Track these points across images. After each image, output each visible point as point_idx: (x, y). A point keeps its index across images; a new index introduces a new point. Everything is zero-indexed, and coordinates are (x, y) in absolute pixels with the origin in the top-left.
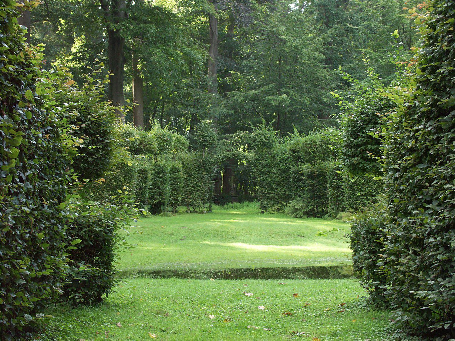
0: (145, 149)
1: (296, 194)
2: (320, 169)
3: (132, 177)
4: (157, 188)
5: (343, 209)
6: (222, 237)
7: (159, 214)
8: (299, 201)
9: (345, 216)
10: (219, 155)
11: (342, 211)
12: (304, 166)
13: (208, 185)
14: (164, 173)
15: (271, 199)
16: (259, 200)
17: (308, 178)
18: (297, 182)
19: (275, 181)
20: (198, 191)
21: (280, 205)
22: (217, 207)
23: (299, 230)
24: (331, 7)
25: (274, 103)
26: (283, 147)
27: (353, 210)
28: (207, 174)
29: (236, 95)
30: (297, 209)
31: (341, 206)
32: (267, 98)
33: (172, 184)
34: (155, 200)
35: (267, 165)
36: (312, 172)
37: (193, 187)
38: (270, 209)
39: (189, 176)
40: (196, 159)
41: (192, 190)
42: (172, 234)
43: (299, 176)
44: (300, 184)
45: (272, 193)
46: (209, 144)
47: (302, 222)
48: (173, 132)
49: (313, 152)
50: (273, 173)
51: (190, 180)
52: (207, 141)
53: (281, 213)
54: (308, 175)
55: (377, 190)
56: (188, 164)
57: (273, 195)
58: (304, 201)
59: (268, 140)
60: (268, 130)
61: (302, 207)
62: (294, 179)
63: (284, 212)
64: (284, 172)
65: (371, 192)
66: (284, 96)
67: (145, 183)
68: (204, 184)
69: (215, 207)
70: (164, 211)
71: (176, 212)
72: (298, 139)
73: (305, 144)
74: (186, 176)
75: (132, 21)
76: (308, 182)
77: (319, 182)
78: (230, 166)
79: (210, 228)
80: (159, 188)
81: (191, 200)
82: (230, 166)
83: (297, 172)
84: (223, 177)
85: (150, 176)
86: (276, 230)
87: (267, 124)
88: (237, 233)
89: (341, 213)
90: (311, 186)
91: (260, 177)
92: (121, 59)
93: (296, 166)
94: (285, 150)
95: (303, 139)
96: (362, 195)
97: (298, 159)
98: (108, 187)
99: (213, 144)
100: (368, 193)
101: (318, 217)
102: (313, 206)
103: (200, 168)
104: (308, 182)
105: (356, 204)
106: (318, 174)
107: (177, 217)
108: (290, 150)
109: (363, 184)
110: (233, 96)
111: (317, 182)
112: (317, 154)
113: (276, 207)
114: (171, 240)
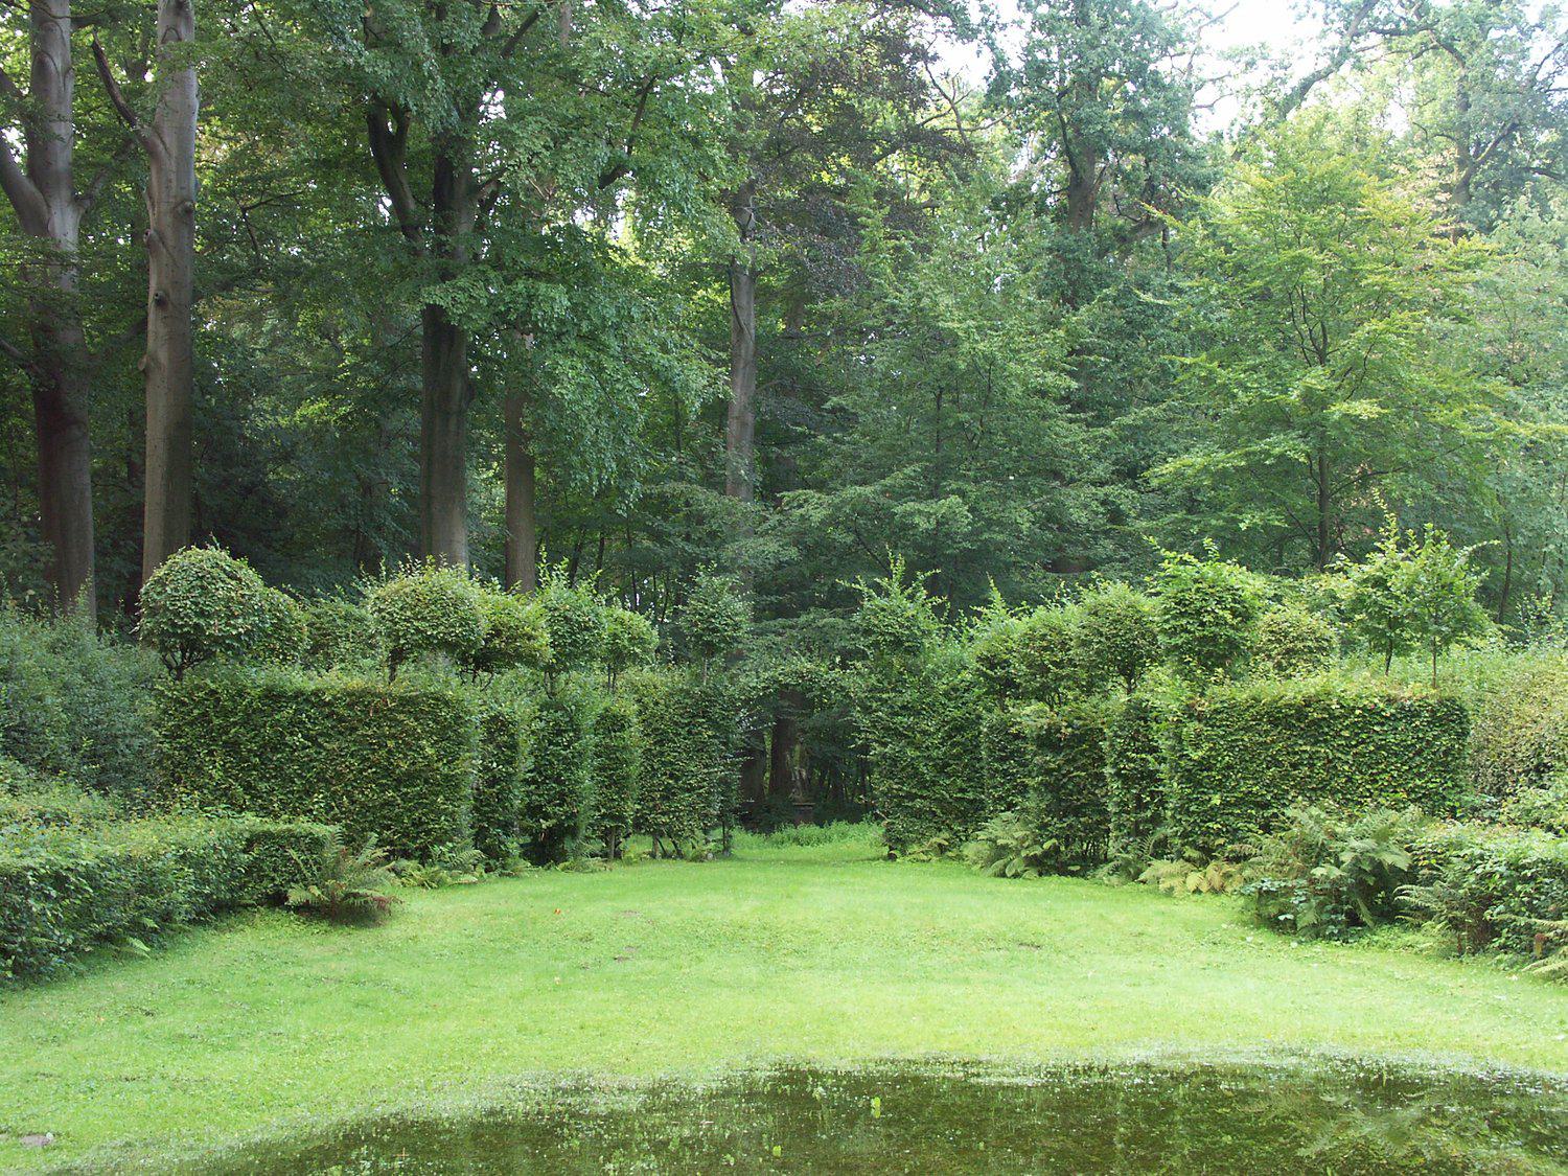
0: (511, 652)
1: (1001, 798)
2: (1079, 718)
3: (461, 743)
4: (550, 775)
5: (1161, 850)
6: (759, 949)
7: (557, 863)
8: (1008, 822)
9: (1172, 875)
10: (752, 678)
11: (1158, 856)
12: (1028, 710)
13: (719, 772)
14: (574, 731)
15: (918, 814)
16: (877, 817)
17: (1040, 746)
18: (1002, 760)
19: (929, 758)
20: (688, 791)
21: (946, 835)
22: (748, 837)
23: (1022, 925)
24: (1086, 254)
25: (923, 524)
26: (954, 650)
27: (1195, 854)
28: (714, 737)
29: (806, 501)
31: (1152, 840)
32: (899, 509)
33: (602, 769)
34: (547, 817)
35: (904, 707)
36: (1054, 729)
37: (671, 776)
38: (916, 848)
39: (660, 743)
40: (681, 690)
41: (668, 788)
42: (588, 938)
43: (1009, 741)
45: (921, 797)
46: (723, 640)
48: (609, 602)
49: (1054, 663)
50: (924, 733)
51: (662, 754)
52: (715, 630)
53: (951, 858)
54: (1039, 736)
55: (1275, 786)
56: (657, 704)
57: (926, 803)
58: (1026, 823)
59: (908, 628)
60: (911, 598)
61: (1023, 839)
62: (991, 751)
63: (960, 858)
64: (959, 729)
65: (1256, 795)
66: (954, 499)
67: (510, 762)
68: (706, 766)
69: (739, 836)
70: (577, 853)
71: (618, 855)
72: (1002, 626)
73: (1030, 637)
74: (648, 742)
75: (492, 274)
76: (1038, 760)
77: (1074, 760)
78: (790, 714)
79: (718, 916)
81: (664, 819)
82: (790, 714)
83: (1002, 728)
84: (769, 747)
85: (526, 743)
86: (942, 922)
87: (906, 582)
88: (811, 932)
89: (1156, 863)
90: (1049, 772)
91: (885, 745)
92: (458, 386)
93: (997, 711)
94: (962, 659)
95: (1020, 626)
96: (1225, 804)
97: (1005, 688)
98: (383, 777)
99: (735, 639)
100: (1247, 794)
101: (1073, 874)
102: (1057, 837)
103: (694, 716)
104: (1038, 760)
105: (1207, 833)
106: (1073, 735)
107: (617, 873)
108: (980, 659)
109: (1229, 767)
110: (800, 506)
111: (1068, 762)
112: (1068, 670)
113: (934, 840)
114: (582, 960)
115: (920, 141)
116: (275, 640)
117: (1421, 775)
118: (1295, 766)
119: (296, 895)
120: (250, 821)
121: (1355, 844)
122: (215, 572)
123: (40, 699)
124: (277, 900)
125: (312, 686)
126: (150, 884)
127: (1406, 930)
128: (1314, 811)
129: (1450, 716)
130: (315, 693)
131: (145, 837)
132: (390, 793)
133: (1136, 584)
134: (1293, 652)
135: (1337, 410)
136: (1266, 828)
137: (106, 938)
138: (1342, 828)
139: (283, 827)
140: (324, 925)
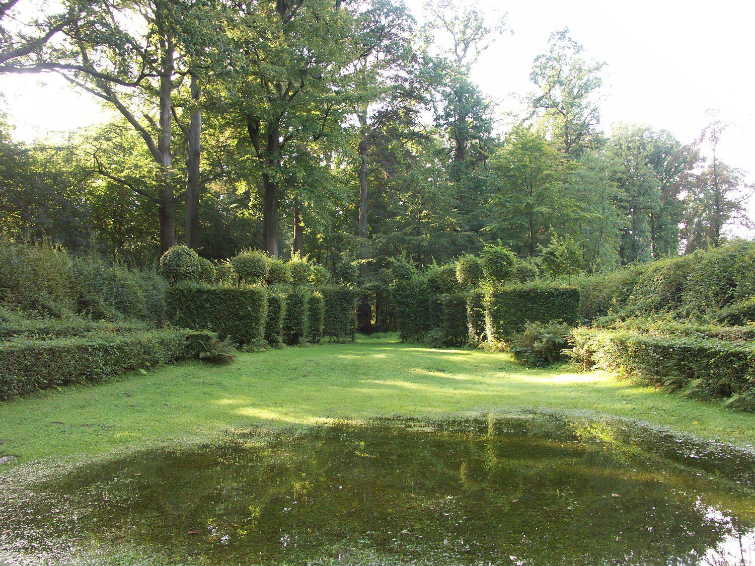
30: (436, 339)
34: (293, 330)
36: (451, 301)
38: (409, 339)
42: (295, 369)
43: (438, 306)
44: (439, 313)
47: (509, 416)
58: (443, 331)
60: (408, 262)
63: (423, 342)
64: (422, 302)
80: (296, 319)
85: (284, 306)
87: (408, 256)
90: (449, 315)
115: (413, 136)
116: (204, 274)
117: (565, 313)
118: (526, 311)
119: (202, 355)
120: (188, 331)
121: (547, 335)
122: (182, 253)
123: (136, 294)
124: (197, 357)
125: (213, 289)
126: (147, 351)
127: (563, 363)
128: (534, 325)
129: (574, 294)
130: (214, 291)
131: (148, 336)
132: (237, 322)
133: (477, 255)
134: (524, 275)
135: (536, 209)
136: (518, 332)
137: (131, 369)
138: (542, 330)
139: (199, 333)
140: (212, 365)
